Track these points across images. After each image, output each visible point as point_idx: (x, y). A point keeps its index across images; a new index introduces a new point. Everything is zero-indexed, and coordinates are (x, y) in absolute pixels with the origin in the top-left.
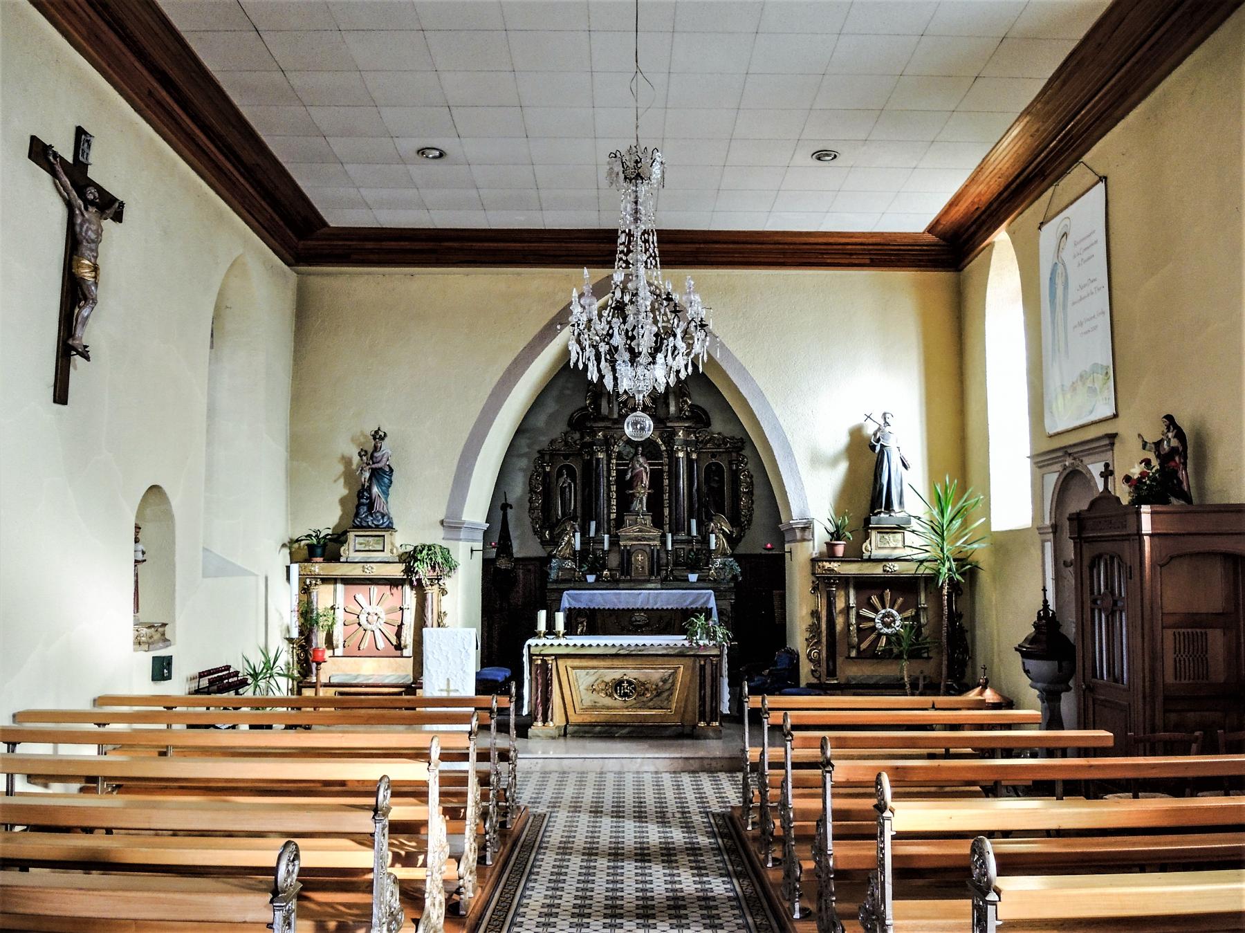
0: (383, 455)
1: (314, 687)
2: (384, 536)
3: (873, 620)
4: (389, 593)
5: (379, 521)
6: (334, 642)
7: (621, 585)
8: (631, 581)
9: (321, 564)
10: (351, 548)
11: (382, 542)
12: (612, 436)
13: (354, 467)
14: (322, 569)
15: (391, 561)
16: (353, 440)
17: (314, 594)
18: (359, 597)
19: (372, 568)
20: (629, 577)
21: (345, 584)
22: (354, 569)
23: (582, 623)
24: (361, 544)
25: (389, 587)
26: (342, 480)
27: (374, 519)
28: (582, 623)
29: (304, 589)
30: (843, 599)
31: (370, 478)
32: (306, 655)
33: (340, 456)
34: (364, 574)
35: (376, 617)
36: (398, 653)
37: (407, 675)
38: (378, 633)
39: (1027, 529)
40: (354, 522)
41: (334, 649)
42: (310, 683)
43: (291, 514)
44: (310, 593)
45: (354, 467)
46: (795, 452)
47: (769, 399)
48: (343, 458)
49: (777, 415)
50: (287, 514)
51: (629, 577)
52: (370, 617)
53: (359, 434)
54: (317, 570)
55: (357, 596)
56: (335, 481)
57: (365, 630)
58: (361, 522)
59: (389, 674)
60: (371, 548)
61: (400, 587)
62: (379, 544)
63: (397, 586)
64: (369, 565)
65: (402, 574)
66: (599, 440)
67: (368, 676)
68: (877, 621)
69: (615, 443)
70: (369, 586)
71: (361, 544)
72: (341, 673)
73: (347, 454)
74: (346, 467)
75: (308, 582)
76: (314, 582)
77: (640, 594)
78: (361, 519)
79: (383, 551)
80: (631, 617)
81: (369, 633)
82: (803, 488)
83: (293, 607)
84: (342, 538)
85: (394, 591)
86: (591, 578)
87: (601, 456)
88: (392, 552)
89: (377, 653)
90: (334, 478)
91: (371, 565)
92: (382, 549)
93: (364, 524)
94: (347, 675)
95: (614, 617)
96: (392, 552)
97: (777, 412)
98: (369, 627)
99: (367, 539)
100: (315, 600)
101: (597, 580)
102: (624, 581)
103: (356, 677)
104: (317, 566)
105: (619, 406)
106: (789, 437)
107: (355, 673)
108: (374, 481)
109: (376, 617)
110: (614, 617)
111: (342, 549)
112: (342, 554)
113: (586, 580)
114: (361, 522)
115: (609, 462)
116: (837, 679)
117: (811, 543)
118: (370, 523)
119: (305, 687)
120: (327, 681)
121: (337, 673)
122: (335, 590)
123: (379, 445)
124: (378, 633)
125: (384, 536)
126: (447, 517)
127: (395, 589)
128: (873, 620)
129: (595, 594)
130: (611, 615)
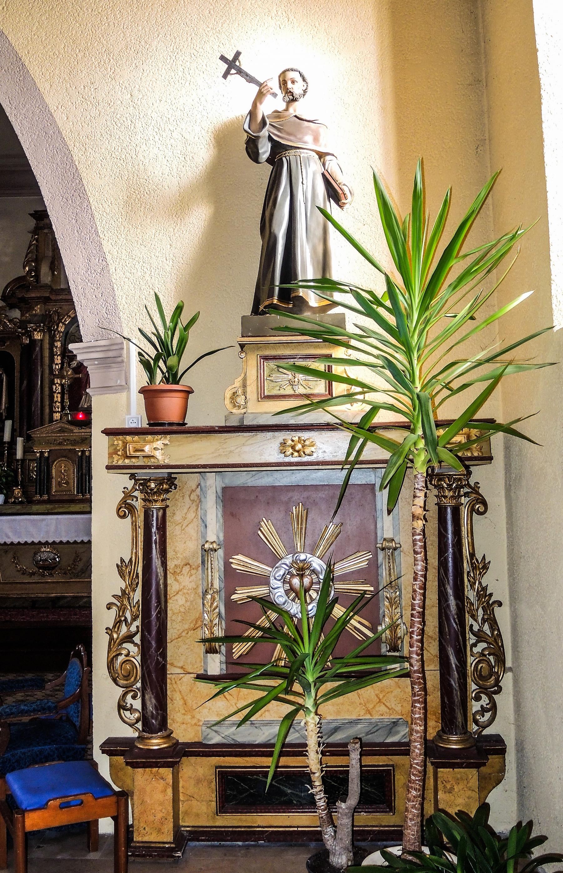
3: (264, 580)
7: (35, 508)
8: (49, 501)
20: (46, 497)
30: (192, 530)
46: (89, 188)
47: (35, 71)
49: (52, 108)
51: (46, 497)
66: (35, 315)
68: (274, 583)
77: (43, 520)
80: (35, 554)
82: (105, 269)
83: (211, 537)
87: (38, 336)
95: (10, 555)
97: (51, 101)
102: (40, 502)
106: (77, 154)
110: (10, 555)
115: (52, 345)
117: (124, 394)
128: (264, 580)
130: (6, 552)
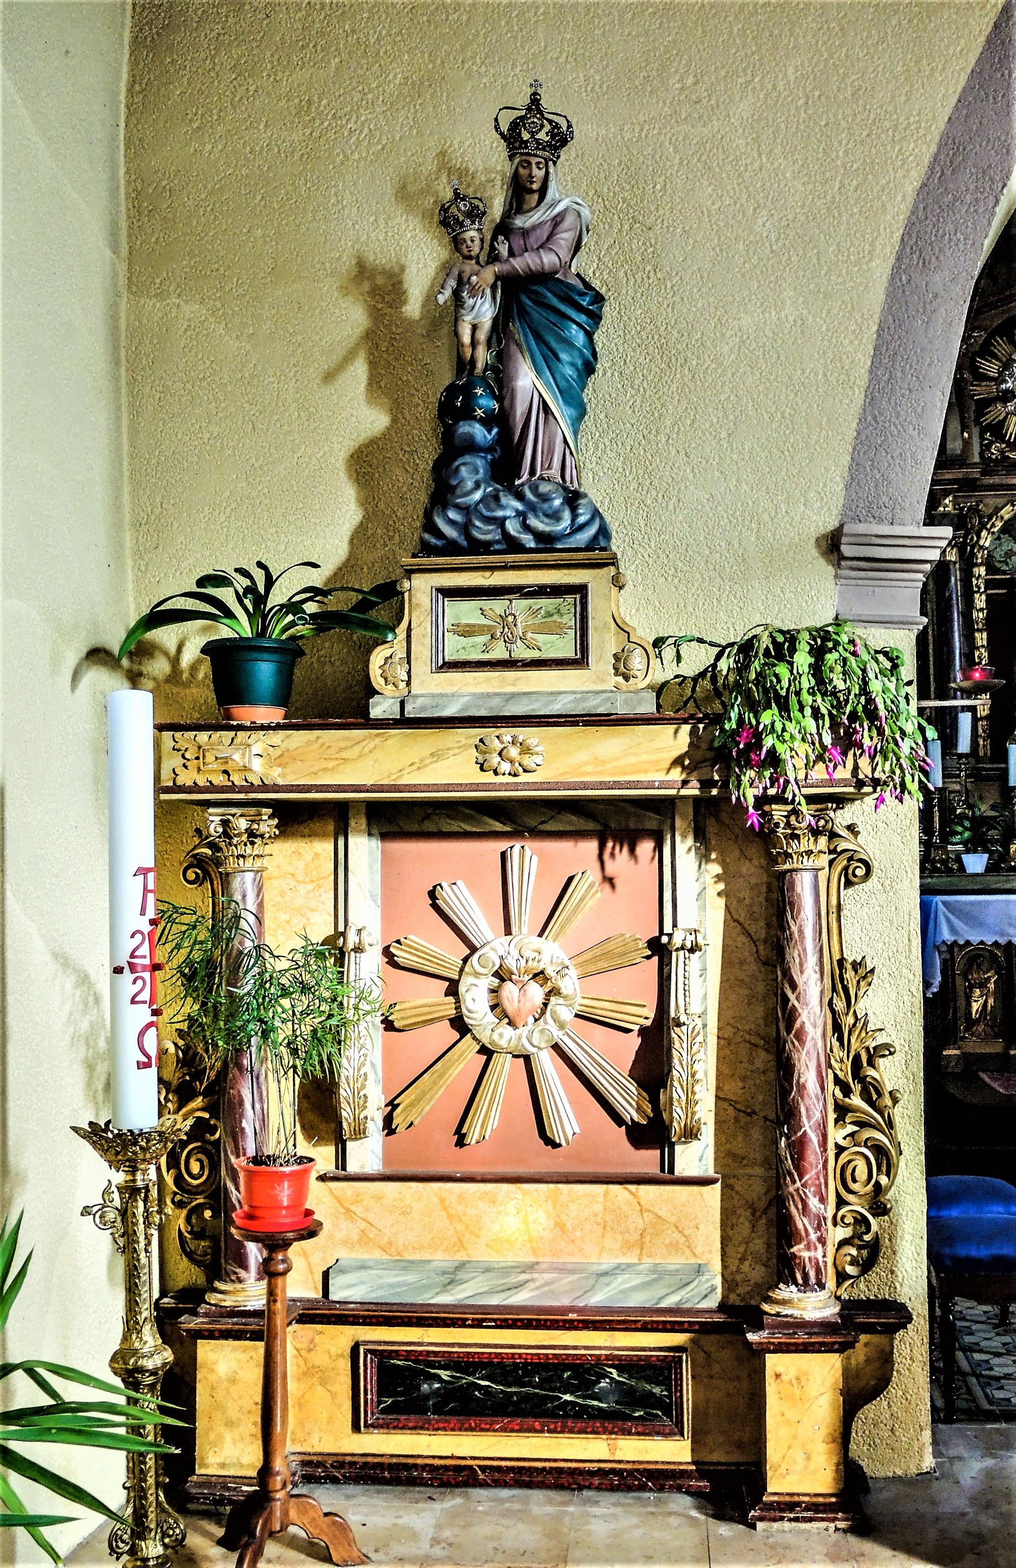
0: (557, 221)
1: (256, 1336)
2: (581, 590)
4: (593, 875)
5: (555, 516)
6: (346, 1113)
9: (277, 737)
10: (422, 650)
11: (569, 620)
12: (975, 510)
13: (413, 308)
14: (281, 760)
15: (621, 709)
16: (404, 194)
17: (243, 884)
18: (454, 898)
19: (526, 750)
21: (384, 836)
22: (436, 755)
23: (983, 985)
24: (467, 631)
25: (592, 846)
26: (359, 370)
27: (532, 508)
28: (983, 985)
29: (199, 862)
31: (500, 327)
32: (215, 1167)
33: (347, 263)
34: (488, 778)
35: (536, 993)
36: (648, 1160)
37: (699, 1270)
38: (547, 1064)
39: (727, 907)
40: (430, 526)
41: (341, 1144)
42: (234, 1313)
43: (137, 525)
44: (226, 879)
45: (413, 308)
48: (363, 271)
50: (117, 526)
52: (509, 990)
53: (430, 166)
54: (257, 765)
55: (447, 896)
56: (329, 376)
57: (487, 1052)
58: (465, 528)
59: (607, 1262)
60: (521, 652)
61: (646, 848)
62: (557, 630)
63: (630, 840)
64: (507, 734)
65: (677, 775)
67: (507, 1270)
69: (983, 526)
70: (503, 845)
71: (467, 631)
72: (377, 1255)
73: (378, 256)
74: (376, 314)
75: (215, 828)
76: (242, 824)
78: (466, 510)
79: (580, 661)
81: (505, 1067)
84: (380, 614)
85: (620, 862)
86: (976, 863)
88: (621, 665)
89: (545, 1160)
90: (327, 364)
91: (523, 733)
92: (565, 647)
93: (484, 532)
94: (408, 1266)
96: (621, 665)
98: (504, 1037)
99: (498, 606)
100: (251, 904)
101: (990, 869)
103: (452, 1277)
104: (259, 742)
105: (982, 438)
107: (442, 1258)
108: (516, 328)
109: (536, 993)
111: (377, 658)
112: (377, 680)
113: (962, 868)
114: (465, 528)
116: (959, 1048)
118: (512, 527)
119: (211, 1335)
120: (312, 1292)
121: (360, 1255)
122: (341, 865)
123: (538, 174)
124: (547, 1064)
125: (581, 590)
126: (851, 512)
127: (623, 855)
129: (1007, 902)
